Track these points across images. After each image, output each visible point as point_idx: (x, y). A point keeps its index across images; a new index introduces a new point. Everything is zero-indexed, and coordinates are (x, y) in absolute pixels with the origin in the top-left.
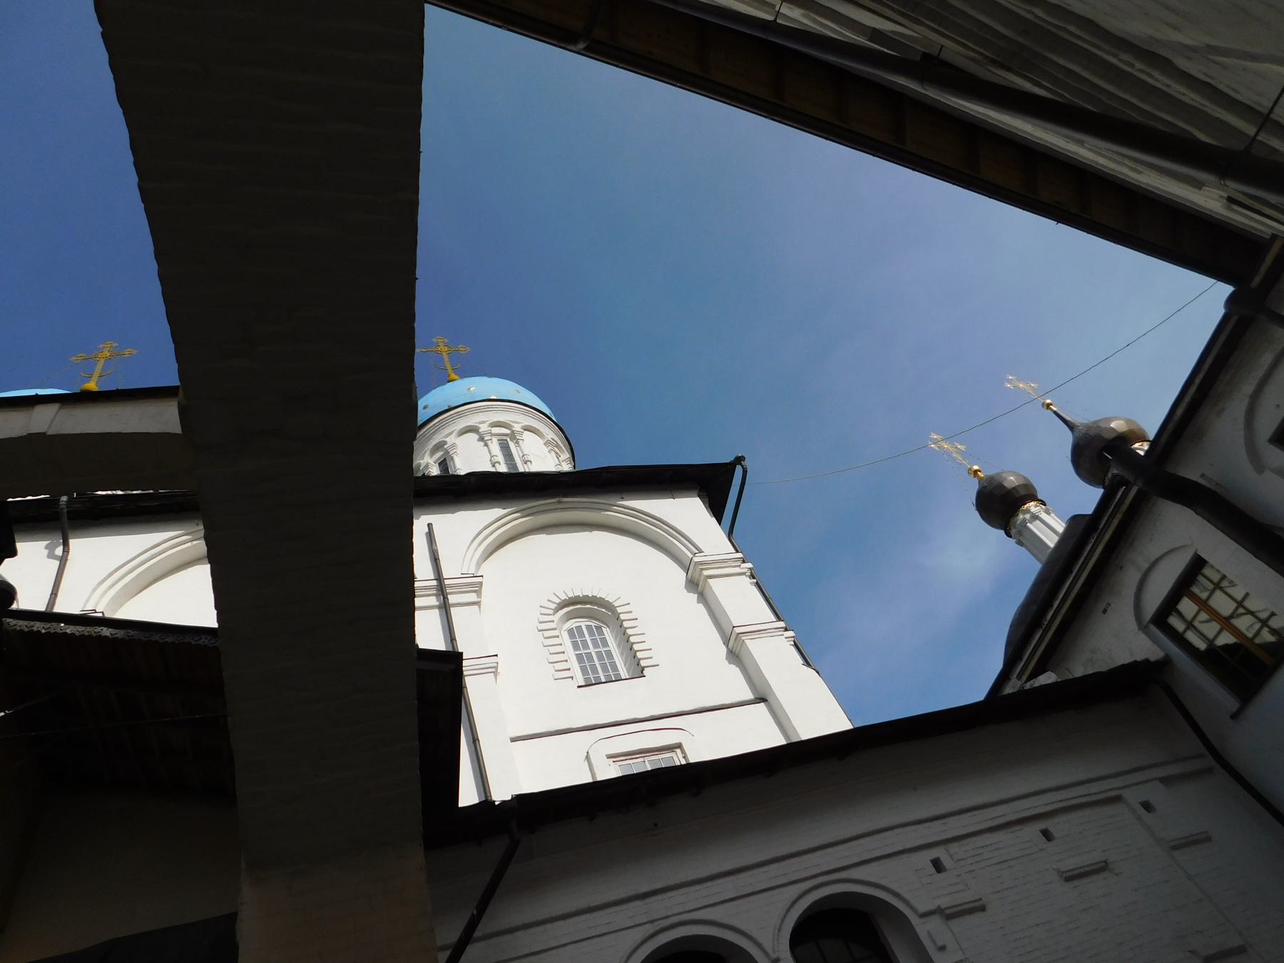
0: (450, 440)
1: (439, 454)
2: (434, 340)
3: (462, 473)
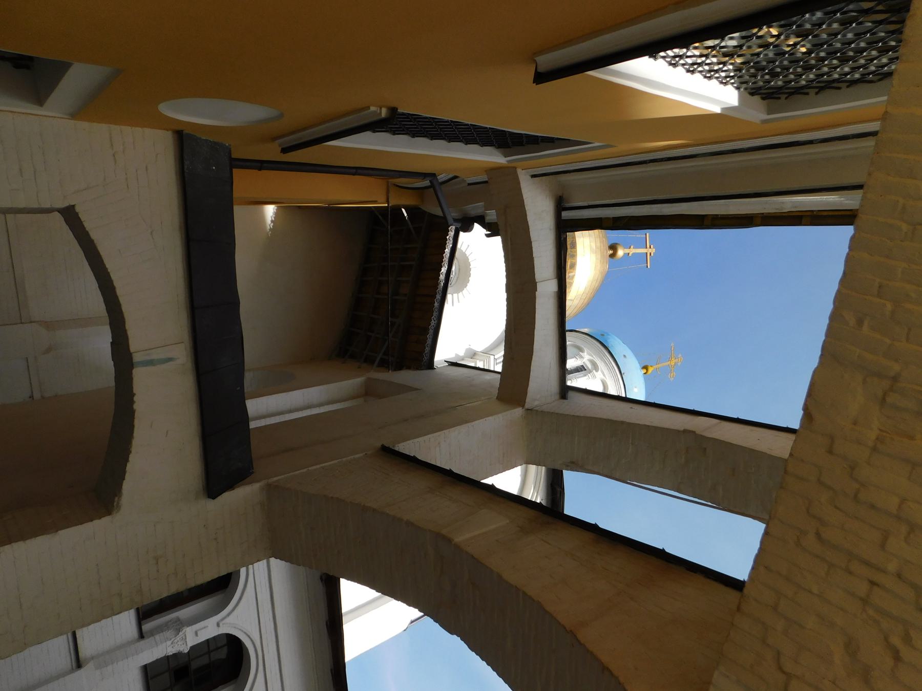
0: (599, 375)
1: (589, 366)
2: (680, 356)
3: (535, 466)
